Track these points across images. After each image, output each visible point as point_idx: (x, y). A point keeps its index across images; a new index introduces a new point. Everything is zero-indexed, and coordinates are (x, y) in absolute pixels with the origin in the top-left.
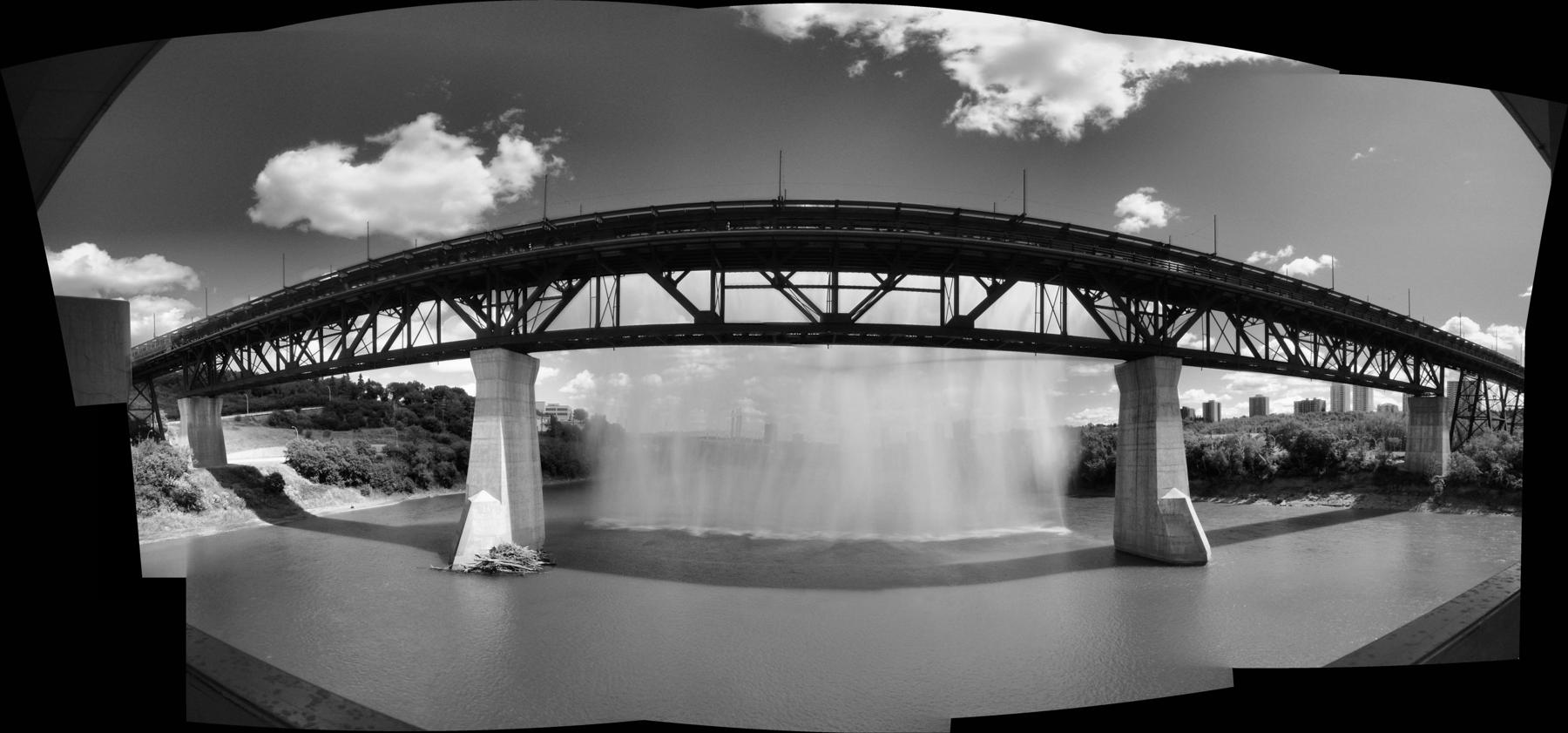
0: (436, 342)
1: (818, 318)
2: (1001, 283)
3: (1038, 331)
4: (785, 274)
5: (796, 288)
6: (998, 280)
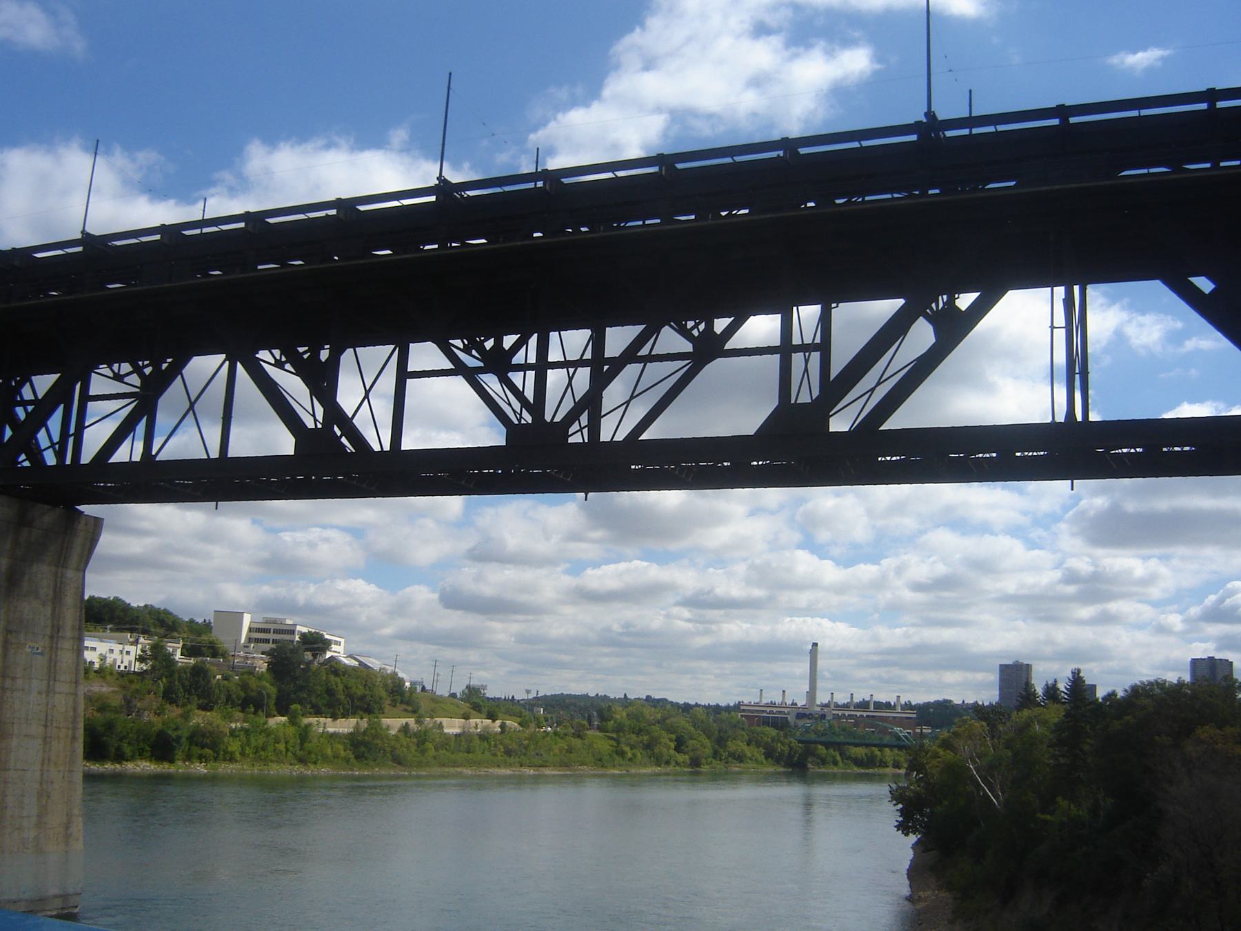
0: (215, 454)
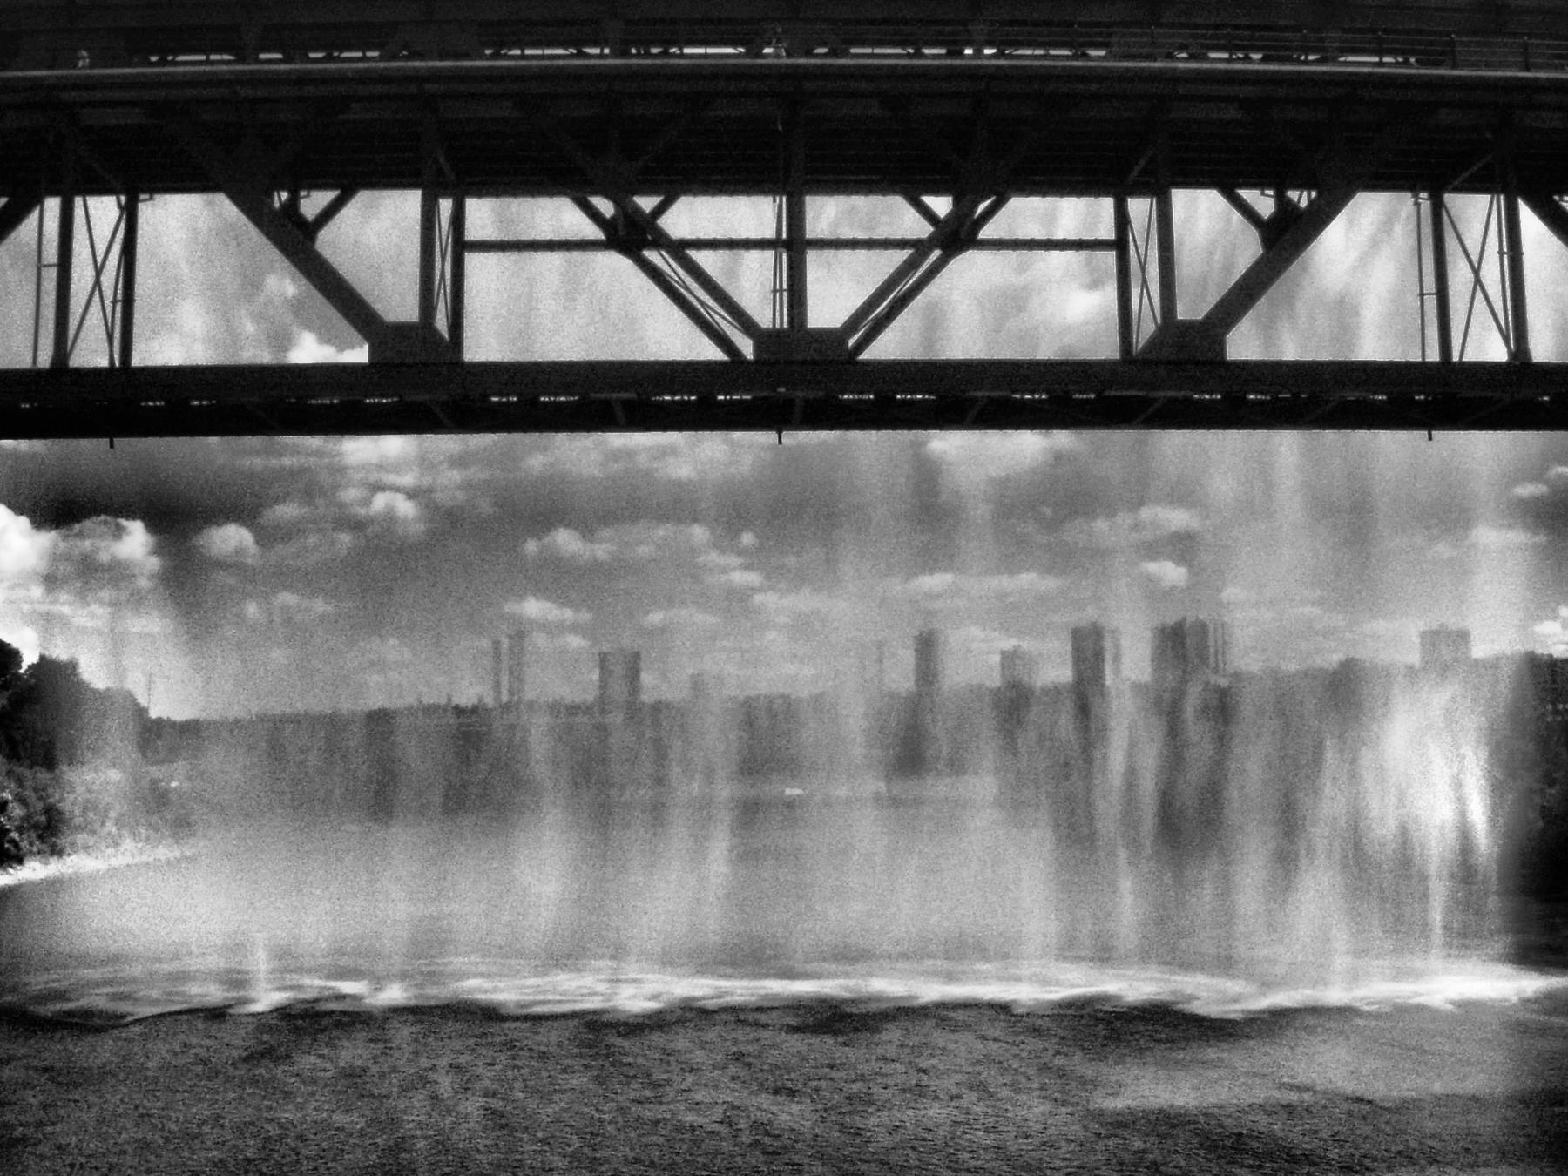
1: (746, 347)
2: (1304, 204)
3: (1434, 355)
4: (647, 203)
5: (679, 249)
6: (1293, 195)
